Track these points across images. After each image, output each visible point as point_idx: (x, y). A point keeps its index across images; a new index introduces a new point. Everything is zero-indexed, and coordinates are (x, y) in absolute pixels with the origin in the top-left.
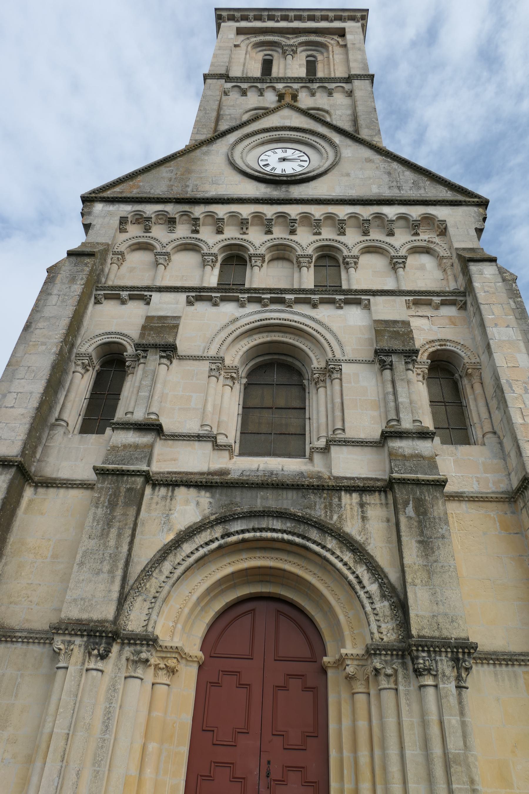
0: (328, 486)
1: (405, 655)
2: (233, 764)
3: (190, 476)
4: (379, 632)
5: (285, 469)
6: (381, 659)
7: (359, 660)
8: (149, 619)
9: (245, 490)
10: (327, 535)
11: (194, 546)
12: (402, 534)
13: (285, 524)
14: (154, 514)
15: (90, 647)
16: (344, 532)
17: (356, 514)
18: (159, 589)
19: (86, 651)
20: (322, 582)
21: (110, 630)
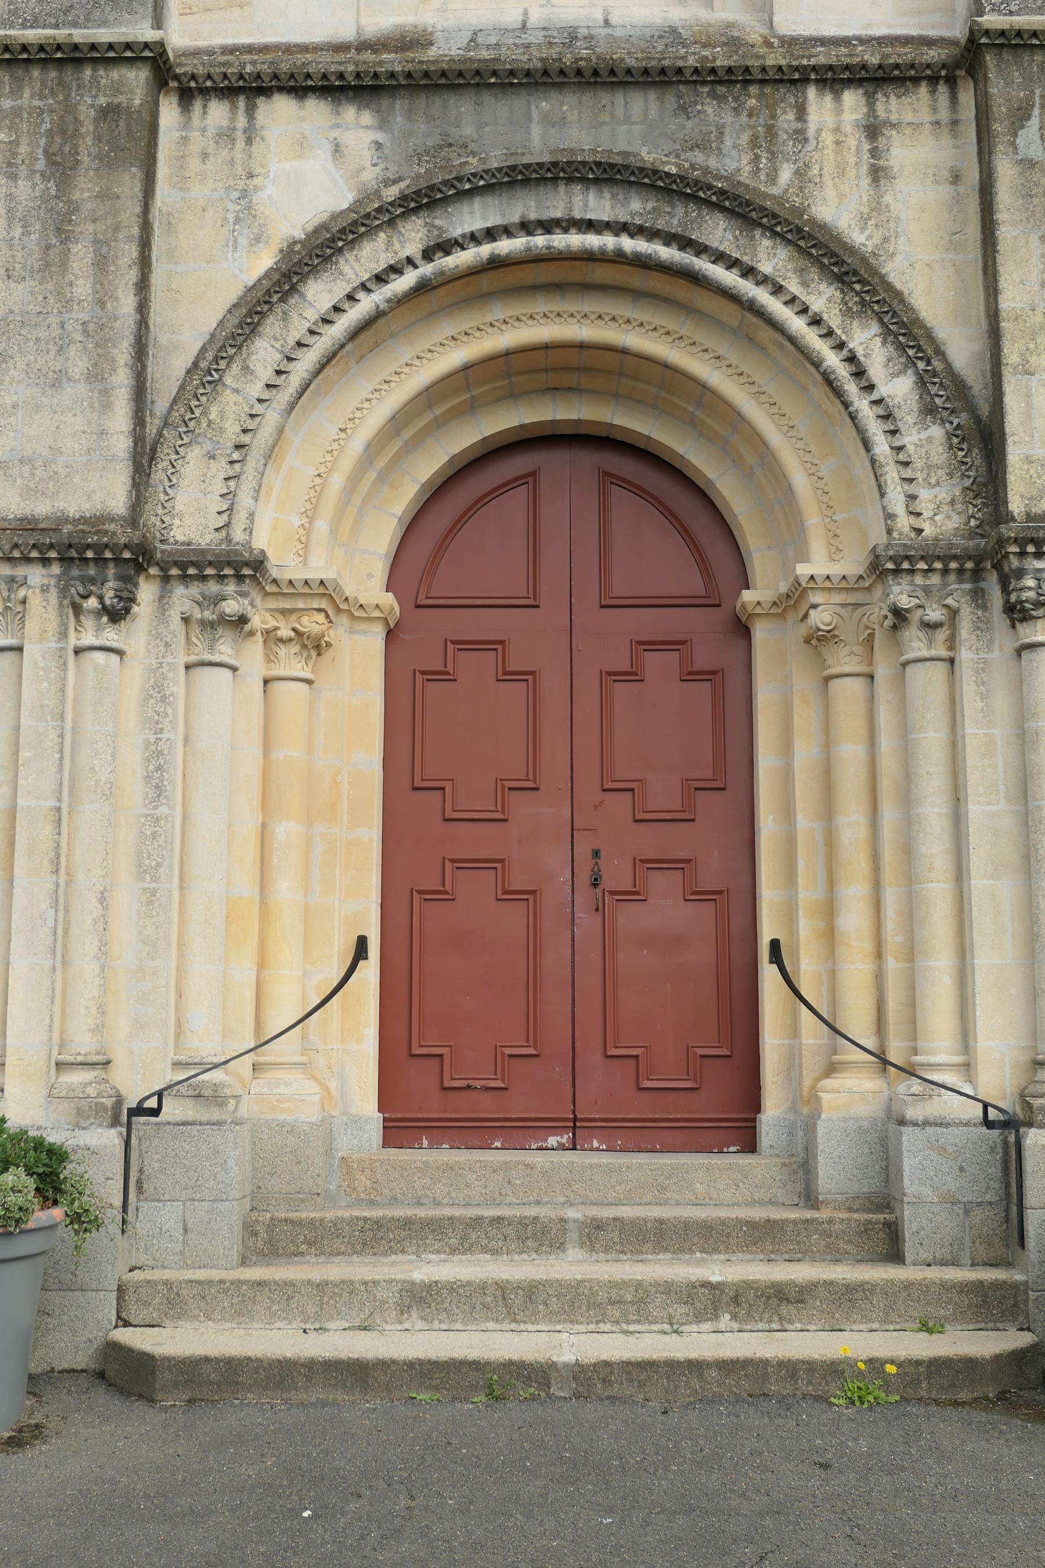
0: (764, 69)
1: (983, 570)
2: (501, 861)
3: (301, 58)
4: (911, 513)
5: (614, 20)
6: (912, 583)
7: (847, 589)
8: (230, 509)
9: (487, 98)
10: (758, 233)
11: (341, 289)
12: (1001, 216)
13: (625, 203)
14: (200, 192)
15: (73, 591)
16: (813, 221)
17: (852, 160)
18: (249, 421)
19: (66, 602)
20: (742, 380)
21: (123, 541)
